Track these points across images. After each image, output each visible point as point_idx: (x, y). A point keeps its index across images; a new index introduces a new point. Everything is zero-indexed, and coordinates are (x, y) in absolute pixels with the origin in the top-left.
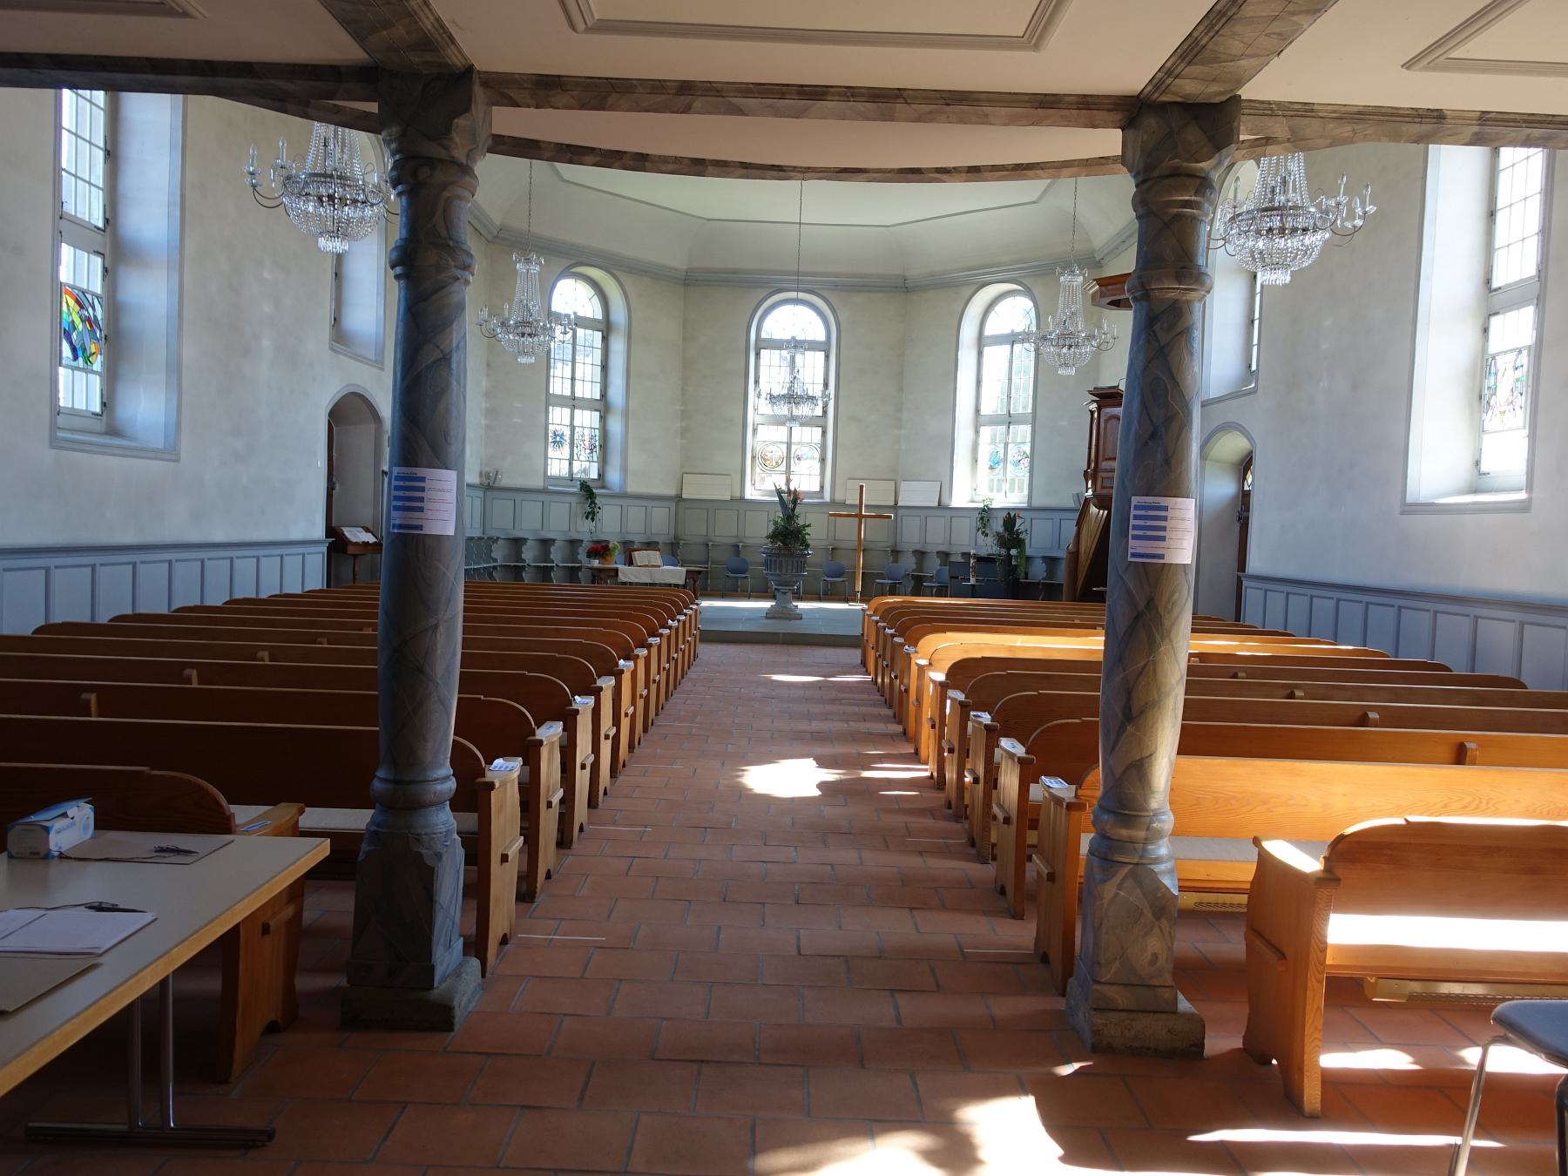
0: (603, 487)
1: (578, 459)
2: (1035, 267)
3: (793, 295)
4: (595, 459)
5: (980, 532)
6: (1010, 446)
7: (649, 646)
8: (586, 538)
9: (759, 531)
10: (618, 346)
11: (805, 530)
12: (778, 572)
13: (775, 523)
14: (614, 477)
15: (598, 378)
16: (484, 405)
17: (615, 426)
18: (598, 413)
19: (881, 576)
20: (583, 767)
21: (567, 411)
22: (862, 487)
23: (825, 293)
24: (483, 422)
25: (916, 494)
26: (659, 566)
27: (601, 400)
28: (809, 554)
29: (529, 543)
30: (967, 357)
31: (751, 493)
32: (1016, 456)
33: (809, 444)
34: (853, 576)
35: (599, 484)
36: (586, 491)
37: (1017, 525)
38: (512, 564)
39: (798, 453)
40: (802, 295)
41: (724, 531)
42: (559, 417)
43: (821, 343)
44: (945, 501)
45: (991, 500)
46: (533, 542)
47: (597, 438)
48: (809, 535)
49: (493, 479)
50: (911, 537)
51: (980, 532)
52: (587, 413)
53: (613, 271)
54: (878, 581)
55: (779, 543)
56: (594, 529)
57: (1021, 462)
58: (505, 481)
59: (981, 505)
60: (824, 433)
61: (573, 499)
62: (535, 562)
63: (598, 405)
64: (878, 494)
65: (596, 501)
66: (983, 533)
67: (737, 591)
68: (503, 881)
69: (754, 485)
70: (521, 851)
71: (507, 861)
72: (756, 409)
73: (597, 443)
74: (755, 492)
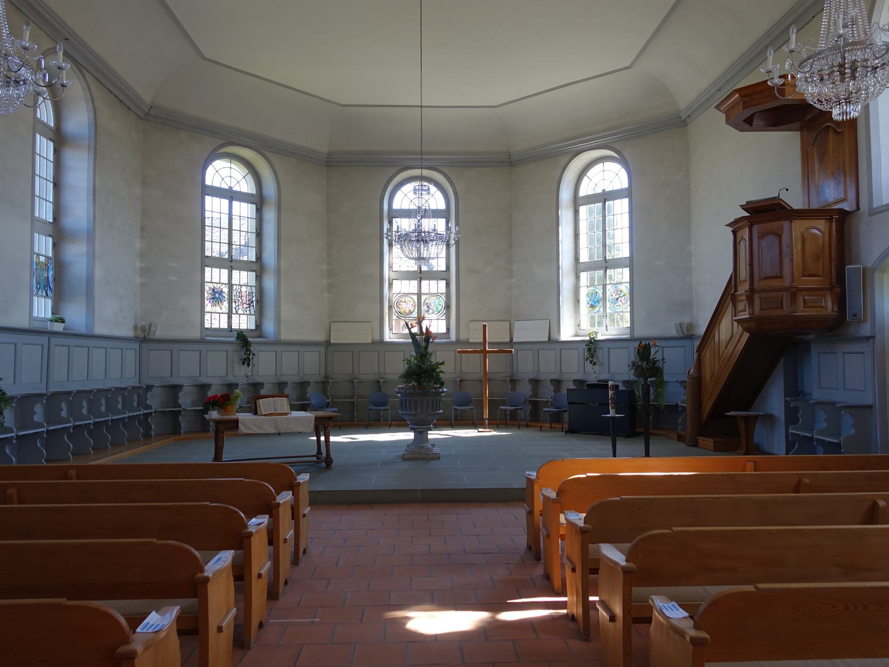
0: (261, 336)
1: (237, 313)
2: (624, 132)
3: (417, 172)
4: (253, 312)
5: (588, 361)
6: (608, 287)
7: (271, 509)
8: (242, 381)
9: (396, 367)
10: (270, 215)
11: (438, 368)
12: (413, 412)
13: (409, 362)
14: (269, 327)
15: (253, 243)
16: (138, 264)
17: (269, 283)
18: (254, 273)
19: (503, 403)
20: (220, 629)
21: (225, 272)
22: (485, 326)
23: (614, 146)
24: (138, 280)
25: (526, 332)
26: (287, 414)
27: (257, 262)
28: (444, 392)
29: (185, 389)
30: (565, 216)
31: (388, 337)
32: (614, 295)
33: (436, 295)
34: (480, 404)
35: (257, 334)
36: (243, 340)
37: (652, 353)
38: (168, 410)
39: (428, 301)
40: (426, 173)
41: (368, 369)
42: (215, 276)
43: (442, 211)
44: (554, 336)
45: (596, 333)
46: (160, 389)
47: (254, 294)
48: (443, 372)
49: (147, 331)
50: (526, 367)
51: (588, 361)
52: (244, 274)
53: (263, 151)
54: (501, 407)
55: (414, 383)
56: (250, 374)
57: (619, 300)
58: (159, 333)
59: (588, 338)
60: (448, 285)
61: (230, 348)
62: (192, 406)
63: (255, 267)
64: (497, 334)
65: (252, 349)
66: (591, 362)
67: (380, 420)
68: (258, 590)
69: (391, 329)
70: (269, 571)
71: (222, 631)
72: (390, 267)
73: (254, 299)
74: (392, 336)
